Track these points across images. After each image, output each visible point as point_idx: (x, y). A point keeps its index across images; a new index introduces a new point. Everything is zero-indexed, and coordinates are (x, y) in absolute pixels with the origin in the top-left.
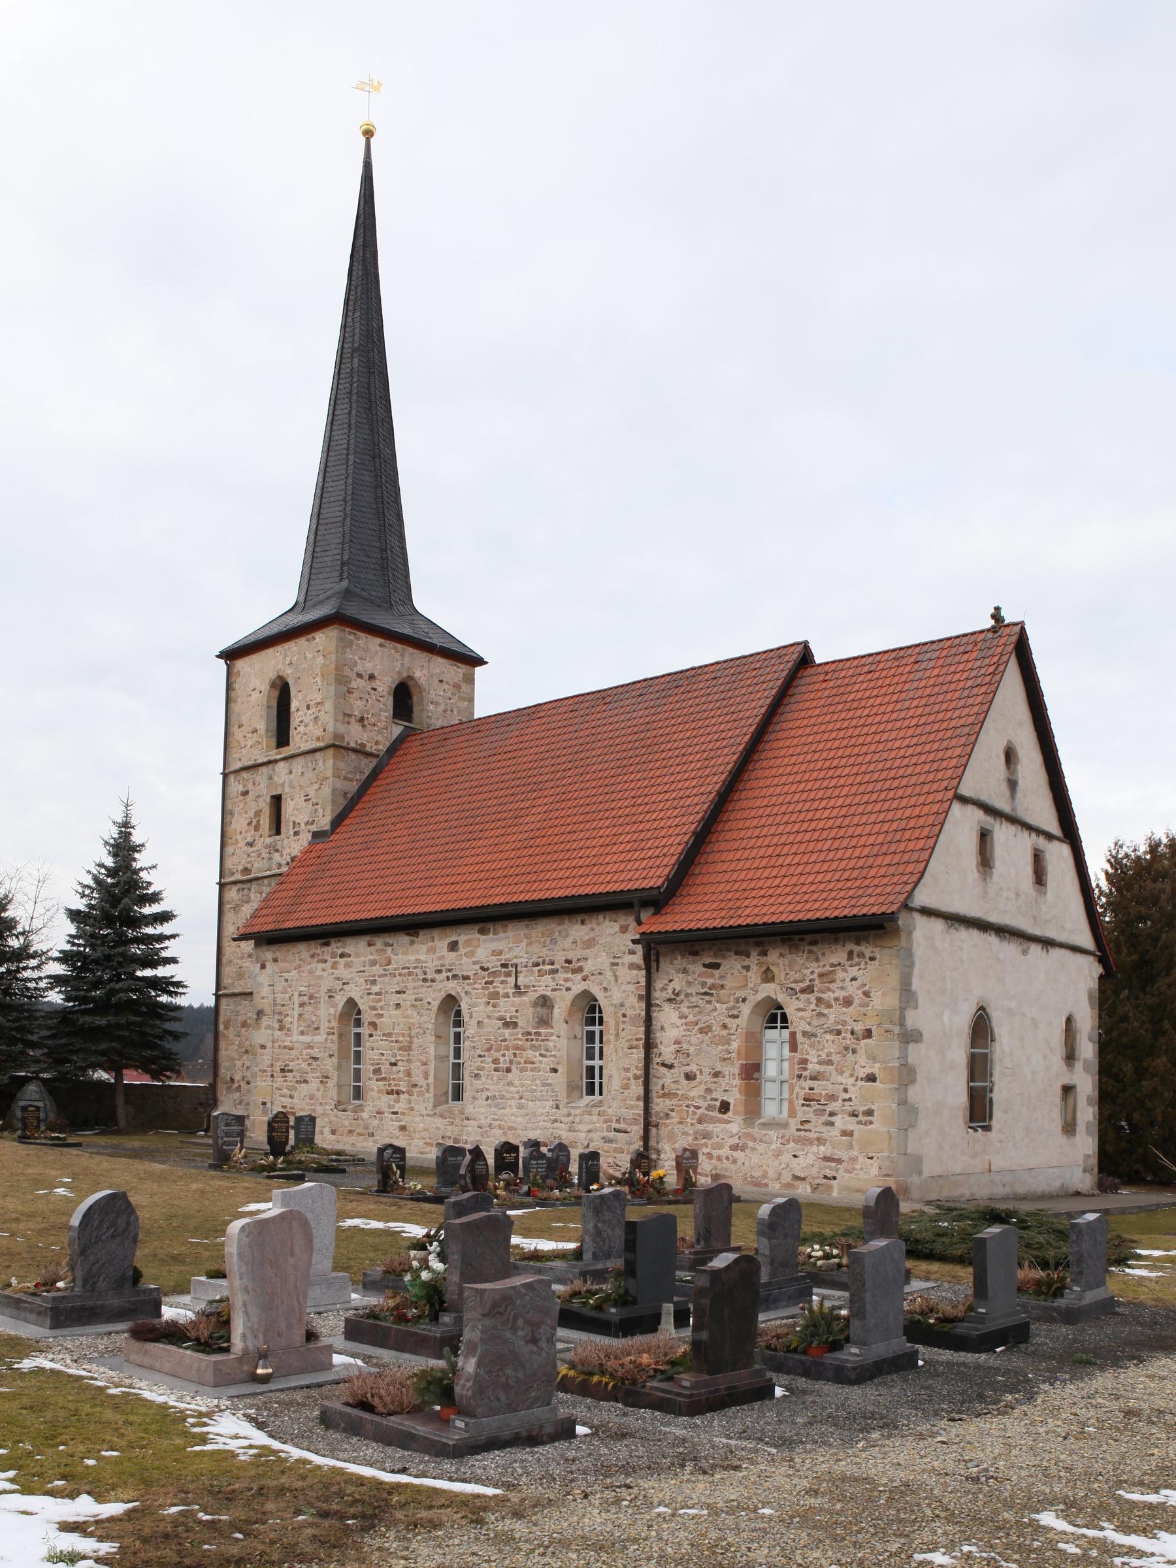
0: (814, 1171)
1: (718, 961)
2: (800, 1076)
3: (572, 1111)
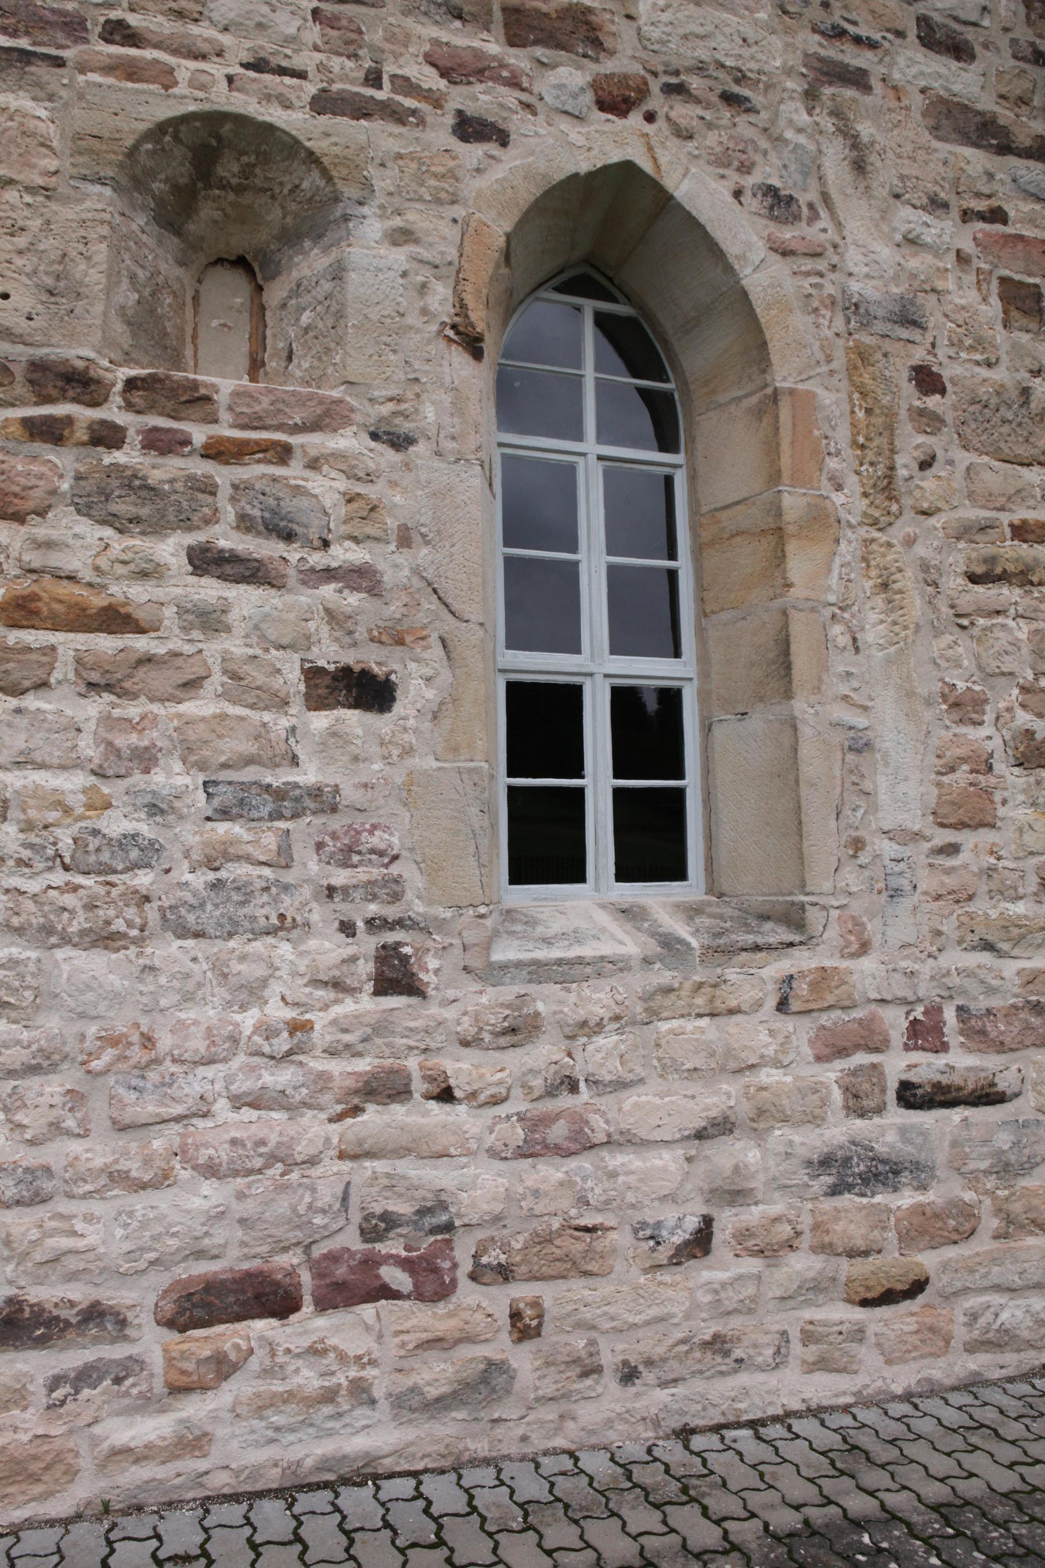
3: (547, 1001)
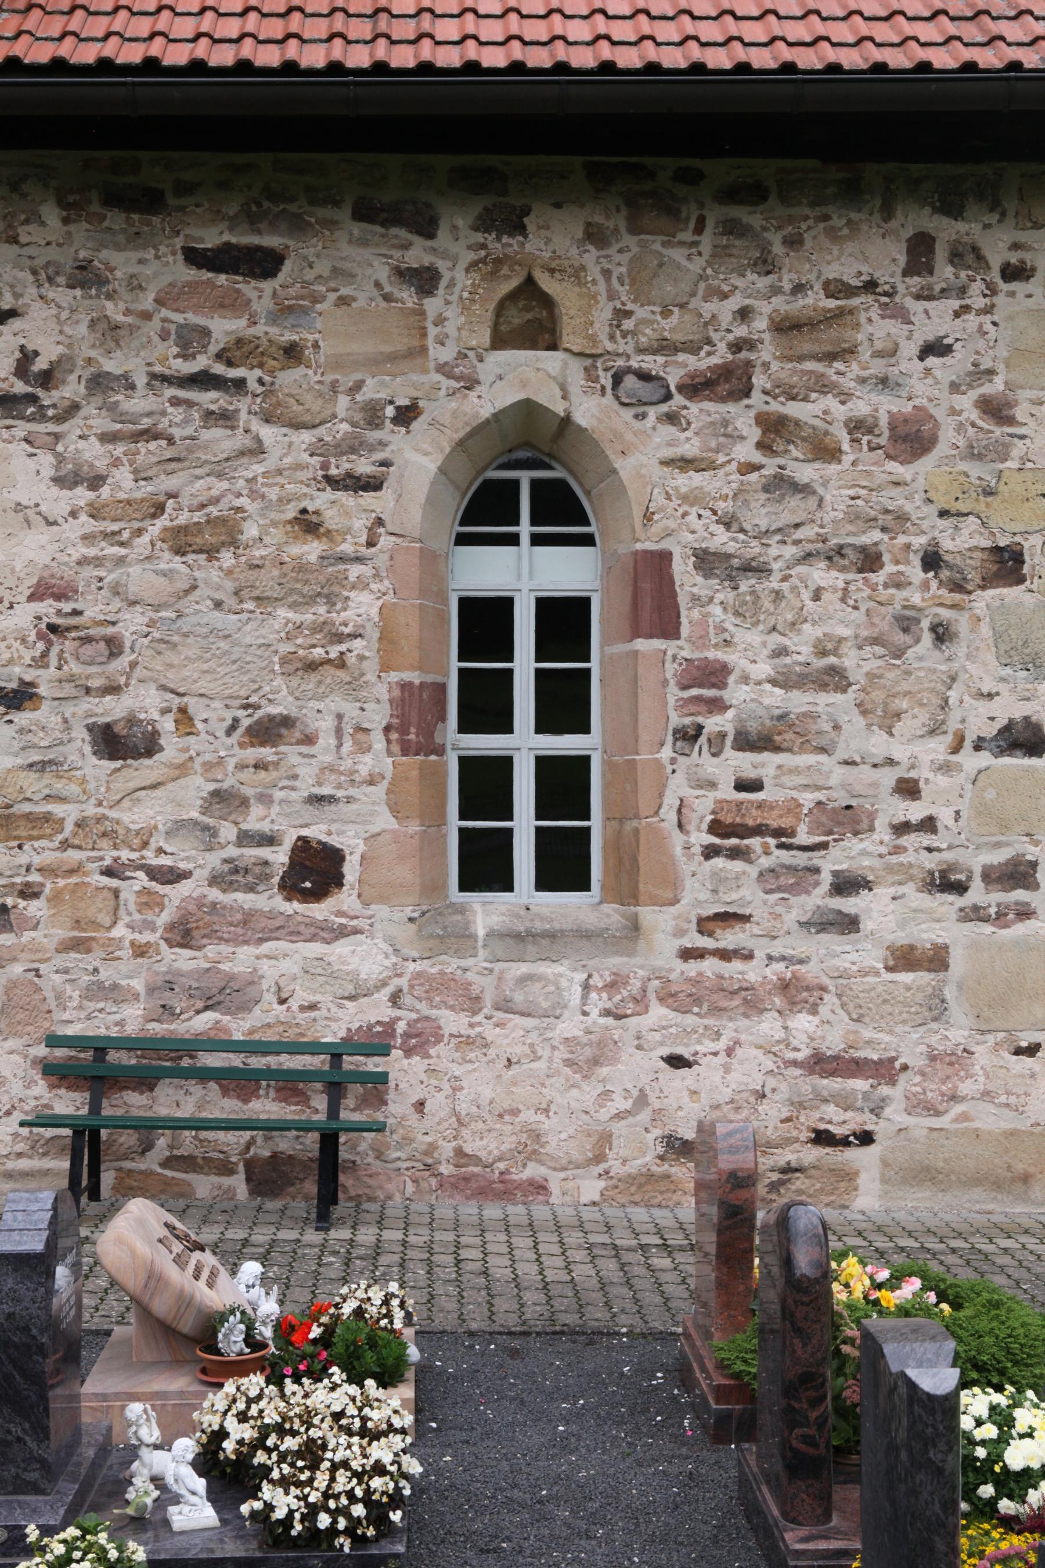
0: (772, 1112)
1: (271, 241)
2: (689, 736)
